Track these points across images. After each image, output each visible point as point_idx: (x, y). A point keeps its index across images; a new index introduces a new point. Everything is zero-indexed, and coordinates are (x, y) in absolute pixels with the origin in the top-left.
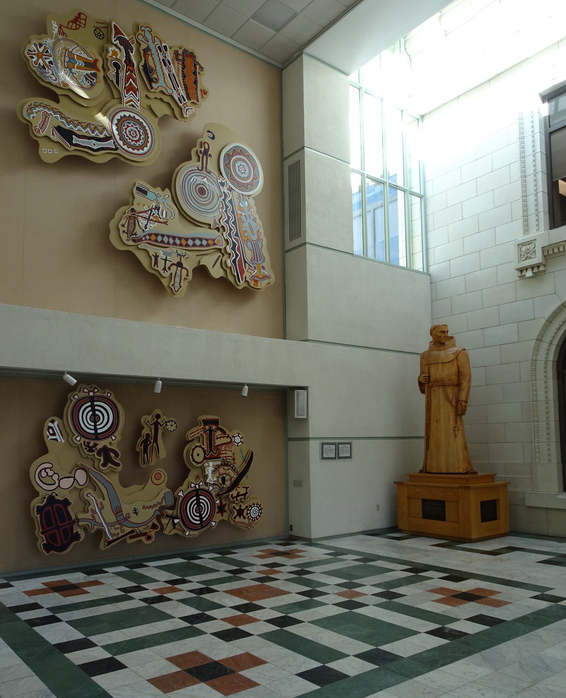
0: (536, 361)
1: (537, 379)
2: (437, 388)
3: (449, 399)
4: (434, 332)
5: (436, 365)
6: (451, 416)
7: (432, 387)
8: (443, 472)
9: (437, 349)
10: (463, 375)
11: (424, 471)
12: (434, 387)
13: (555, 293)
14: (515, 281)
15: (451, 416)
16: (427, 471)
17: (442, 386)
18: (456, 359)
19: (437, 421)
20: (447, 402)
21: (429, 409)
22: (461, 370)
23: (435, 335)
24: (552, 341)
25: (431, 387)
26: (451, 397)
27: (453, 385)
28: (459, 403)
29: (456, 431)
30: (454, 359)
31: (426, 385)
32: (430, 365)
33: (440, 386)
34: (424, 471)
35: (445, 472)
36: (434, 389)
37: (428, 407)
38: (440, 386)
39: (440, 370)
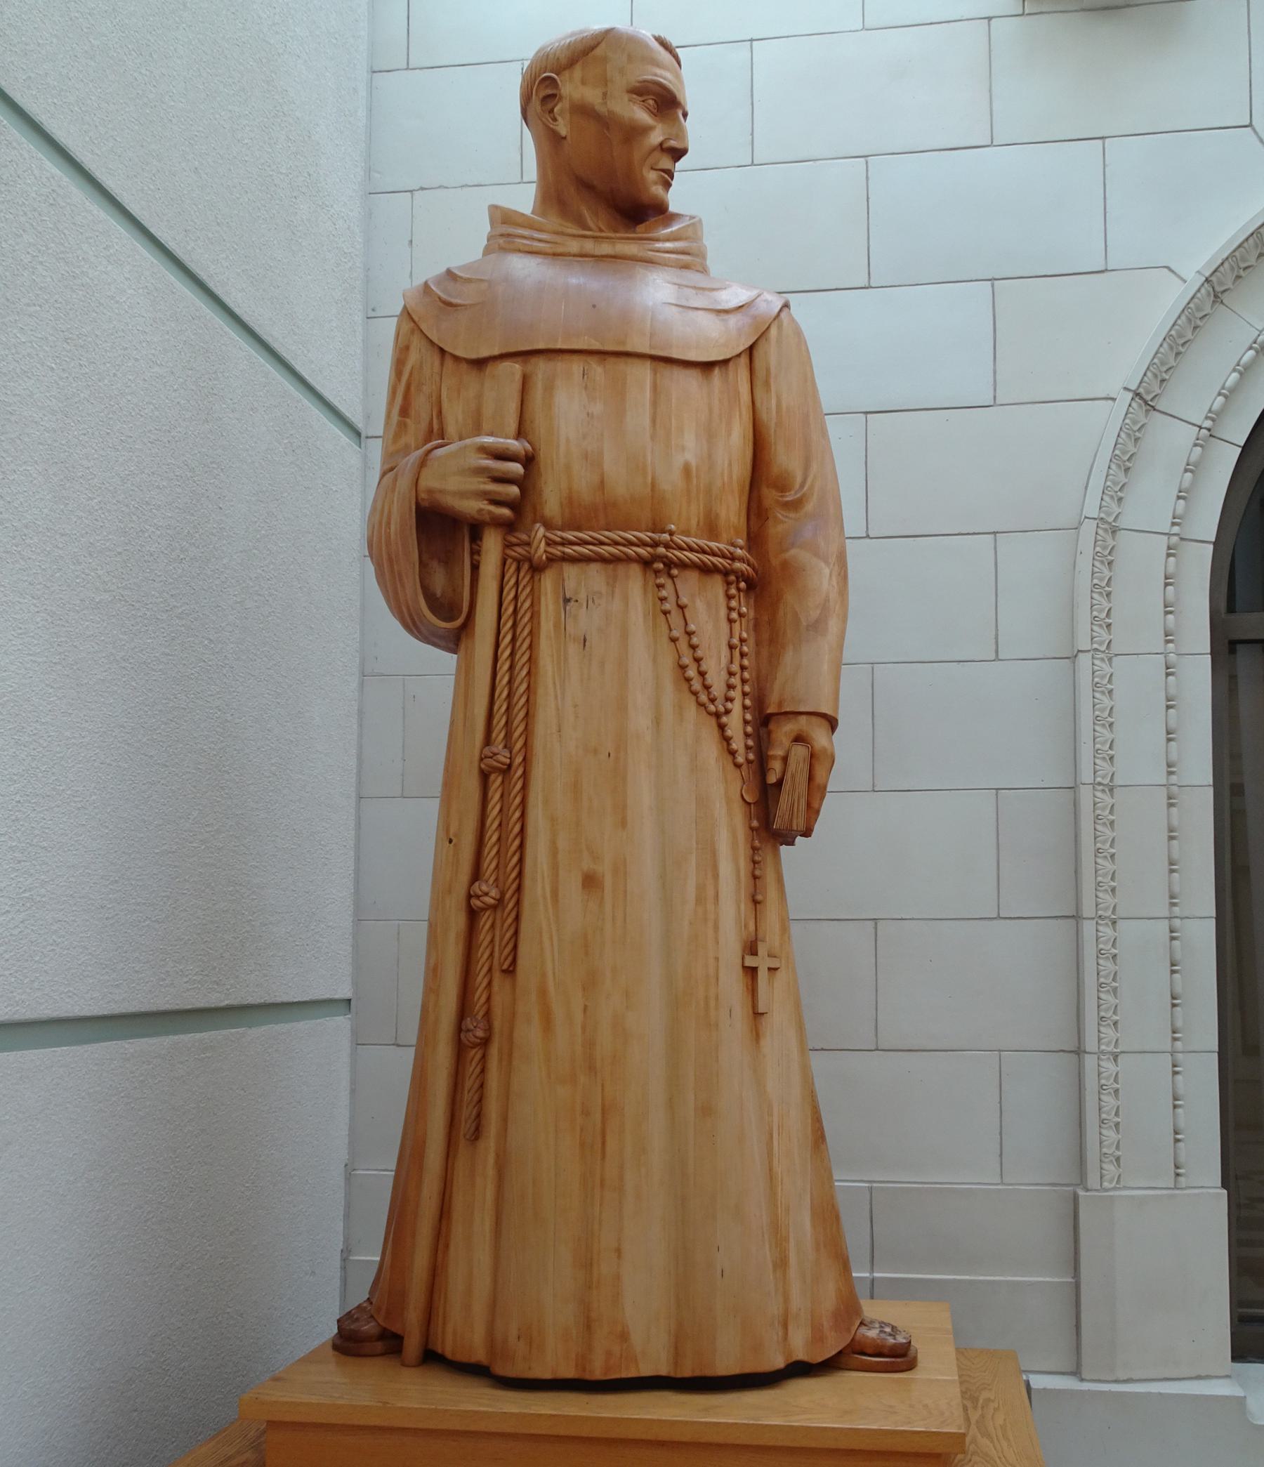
0: (1114, 532)
1: (1115, 649)
2: (595, 576)
3: (707, 688)
4: (573, 88)
5: (598, 370)
6: (724, 847)
7: (551, 560)
8: (646, 1371)
9: (589, 246)
10: (796, 505)
11: (412, 1345)
12: (571, 571)
13: (1250, 125)
14: (990, 19)
15: (724, 847)
16: (448, 1348)
17: (646, 563)
18: (744, 360)
19: (590, 882)
20: (691, 710)
21: (507, 770)
22: (785, 458)
23: (583, 111)
24: (1215, 417)
25: (537, 569)
26: (717, 681)
27: (725, 573)
28: (783, 732)
29: (762, 975)
30: (739, 355)
31: (492, 544)
32: (541, 368)
33: (628, 559)
34: (412, 1345)
35: (663, 1368)
36: (570, 585)
37: (498, 746)
38: (628, 559)
39: (639, 417)
